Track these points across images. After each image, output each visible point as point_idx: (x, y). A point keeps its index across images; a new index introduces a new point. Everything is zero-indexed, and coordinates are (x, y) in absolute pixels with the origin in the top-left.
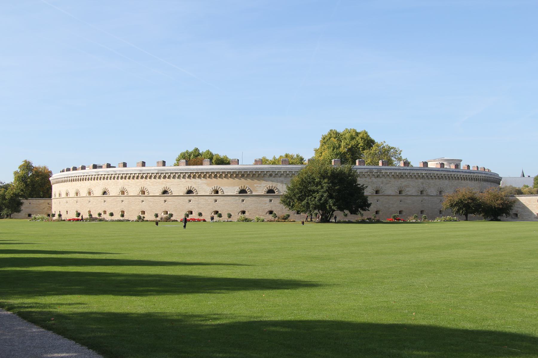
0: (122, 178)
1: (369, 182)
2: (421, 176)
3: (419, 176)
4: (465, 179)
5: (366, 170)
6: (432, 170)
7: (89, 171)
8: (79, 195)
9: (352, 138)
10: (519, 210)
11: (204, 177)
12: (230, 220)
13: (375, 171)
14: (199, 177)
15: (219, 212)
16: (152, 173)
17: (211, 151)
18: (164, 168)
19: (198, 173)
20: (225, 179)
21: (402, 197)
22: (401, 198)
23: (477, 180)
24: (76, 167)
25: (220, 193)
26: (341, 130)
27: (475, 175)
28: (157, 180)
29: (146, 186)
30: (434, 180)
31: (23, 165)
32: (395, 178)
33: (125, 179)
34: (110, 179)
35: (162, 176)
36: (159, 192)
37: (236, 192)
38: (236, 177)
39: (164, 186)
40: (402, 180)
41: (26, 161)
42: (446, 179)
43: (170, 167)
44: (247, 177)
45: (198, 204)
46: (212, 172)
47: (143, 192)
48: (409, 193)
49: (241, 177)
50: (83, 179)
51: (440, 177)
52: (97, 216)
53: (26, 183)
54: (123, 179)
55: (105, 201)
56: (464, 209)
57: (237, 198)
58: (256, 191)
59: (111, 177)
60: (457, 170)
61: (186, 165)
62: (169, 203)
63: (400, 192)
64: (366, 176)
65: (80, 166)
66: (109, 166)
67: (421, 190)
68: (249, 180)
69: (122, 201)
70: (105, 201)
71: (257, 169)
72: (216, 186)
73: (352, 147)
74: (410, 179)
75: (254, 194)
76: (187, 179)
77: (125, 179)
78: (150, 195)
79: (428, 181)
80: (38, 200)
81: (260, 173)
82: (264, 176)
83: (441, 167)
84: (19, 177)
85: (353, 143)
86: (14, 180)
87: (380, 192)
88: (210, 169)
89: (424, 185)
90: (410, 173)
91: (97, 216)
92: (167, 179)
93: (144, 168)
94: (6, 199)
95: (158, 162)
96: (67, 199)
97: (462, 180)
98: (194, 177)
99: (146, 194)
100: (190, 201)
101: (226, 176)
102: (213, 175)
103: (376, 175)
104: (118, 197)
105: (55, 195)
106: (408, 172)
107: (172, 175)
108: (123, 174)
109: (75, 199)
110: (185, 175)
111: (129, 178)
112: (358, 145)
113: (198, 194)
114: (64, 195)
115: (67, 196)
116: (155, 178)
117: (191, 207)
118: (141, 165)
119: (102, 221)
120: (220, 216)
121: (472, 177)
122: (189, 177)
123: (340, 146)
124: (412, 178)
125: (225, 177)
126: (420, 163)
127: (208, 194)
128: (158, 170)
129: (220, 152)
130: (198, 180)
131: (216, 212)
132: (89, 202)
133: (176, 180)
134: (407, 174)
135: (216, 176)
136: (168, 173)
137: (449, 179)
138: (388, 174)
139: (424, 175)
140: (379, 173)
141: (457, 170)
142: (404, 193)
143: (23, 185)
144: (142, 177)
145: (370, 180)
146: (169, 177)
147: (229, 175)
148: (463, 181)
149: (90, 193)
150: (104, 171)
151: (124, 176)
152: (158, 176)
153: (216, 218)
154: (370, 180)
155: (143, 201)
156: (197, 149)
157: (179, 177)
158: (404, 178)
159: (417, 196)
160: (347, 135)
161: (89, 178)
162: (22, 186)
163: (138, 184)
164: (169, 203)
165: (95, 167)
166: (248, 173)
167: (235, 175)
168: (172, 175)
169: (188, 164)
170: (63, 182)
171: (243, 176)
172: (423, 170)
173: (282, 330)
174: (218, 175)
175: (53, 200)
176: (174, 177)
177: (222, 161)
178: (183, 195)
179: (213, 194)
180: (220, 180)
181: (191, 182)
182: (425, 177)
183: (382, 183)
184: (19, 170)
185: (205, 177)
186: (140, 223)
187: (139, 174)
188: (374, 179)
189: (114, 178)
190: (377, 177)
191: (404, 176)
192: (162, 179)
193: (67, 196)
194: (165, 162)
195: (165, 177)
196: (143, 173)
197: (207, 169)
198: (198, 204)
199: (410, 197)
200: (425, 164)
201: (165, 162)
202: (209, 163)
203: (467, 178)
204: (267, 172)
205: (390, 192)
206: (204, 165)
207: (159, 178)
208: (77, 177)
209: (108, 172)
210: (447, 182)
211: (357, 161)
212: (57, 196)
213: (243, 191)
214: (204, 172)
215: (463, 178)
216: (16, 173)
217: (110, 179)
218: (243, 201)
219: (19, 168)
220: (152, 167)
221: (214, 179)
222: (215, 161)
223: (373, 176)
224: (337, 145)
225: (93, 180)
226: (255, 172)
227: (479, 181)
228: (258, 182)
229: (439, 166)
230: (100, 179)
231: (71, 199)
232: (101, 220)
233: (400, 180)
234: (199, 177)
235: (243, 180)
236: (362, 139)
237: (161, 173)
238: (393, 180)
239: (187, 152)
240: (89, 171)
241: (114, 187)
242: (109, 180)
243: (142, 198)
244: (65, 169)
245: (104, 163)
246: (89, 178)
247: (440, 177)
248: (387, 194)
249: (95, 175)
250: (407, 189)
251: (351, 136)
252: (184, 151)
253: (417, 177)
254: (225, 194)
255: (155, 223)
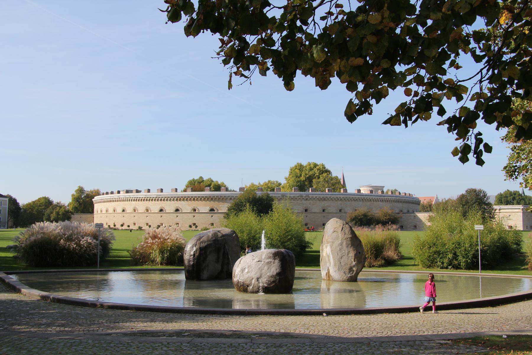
0: (134, 200)
1: (300, 204)
2: (340, 199)
3: (338, 199)
4: (377, 200)
5: (298, 195)
6: (363, 195)
7: (123, 195)
8: (116, 211)
9: (311, 169)
10: (418, 223)
11: (186, 200)
12: (197, 229)
13: (304, 196)
14: (183, 200)
15: (196, 224)
16: (153, 197)
17: (212, 178)
18: (162, 193)
19: (182, 197)
20: (200, 202)
21: (324, 214)
22: (324, 214)
23: (387, 202)
24: (108, 192)
25: (197, 211)
26: (304, 163)
27: (386, 198)
28: (157, 202)
29: (149, 206)
30: (351, 202)
31: (78, 190)
32: (319, 200)
33: (136, 201)
34: (127, 201)
35: (160, 199)
36: (157, 211)
37: (207, 211)
38: (207, 200)
39: (160, 206)
40: (325, 202)
41: (80, 187)
42: (360, 201)
43: (180, 193)
44: (215, 200)
45: (183, 218)
46: (191, 197)
47: (147, 210)
48: (330, 211)
49: (211, 200)
50: (119, 200)
51: (356, 200)
52: (113, 227)
53: (79, 202)
54: (135, 201)
55: (123, 216)
56: (359, 222)
57: (208, 214)
58: (221, 209)
59: (127, 200)
60: (372, 194)
61: (192, 191)
62: (164, 218)
63: (324, 211)
64: (298, 199)
65: (110, 192)
66: (137, 191)
67: (340, 209)
68: (216, 202)
69: (134, 216)
70: (123, 216)
71: (221, 195)
72: (194, 206)
73: (310, 176)
74: (331, 201)
75: (219, 211)
76: (176, 202)
77: (136, 201)
78: (152, 212)
79: (345, 202)
80: (86, 215)
81: (223, 197)
82: (226, 200)
83: (358, 192)
84: (75, 198)
85: (311, 173)
86: (71, 200)
87: (308, 210)
88: (190, 195)
89: (342, 205)
90: (331, 197)
91: (113, 227)
92: (163, 202)
93: (149, 194)
94: (60, 215)
95: (158, 190)
96: (101, 215)
97: (374, 201)
98: (180, 200)
99: (149, 212)
100: (177, 216)
101: (201, 200)
102: (192, 199)
103: (305, 199)
104: (132, 214)
105: (97, 212)
106: (330, 196)
107: (166, 199)
108: (135, 198)
109: (106, 215)
110: (184, 198)
111: (139, 201)
112: (314, 175)
113: (183, 212)
114: (104, 212)
115: (107, 212)
116: (155, 200)
117: (178, 221)
118: (147, 191)
119: (116, 230)
120: (196, 227)
121: (392, 199)
122: (177, 200)
123: (301, 175)
124: (333, 200)
125: (200, 200)
126: (355, 190)
127: (189, 212)
128: (157, 195)
129: (218, 179)
130: (182, 202)
131: (194, 224)
132: (114, 217)
133: (169, 202)
134: (328, 198)
135: (194, 200)
136: (163, 197)
137: (363, 201)
138: (314, 197)
139: (342, 198)
140: (307, 197)
141: (359, 194)
142: (326, 211)
143: (78, 204)
144: (147, 200)
145: (301, 202)
146: (164, 200)
147: (203, 199)
148: (375, 203)
149: (135, 211)
150: (134, 195)
151: (135, 199)
152: (157, 199)
153: (194, 227)
154: (301, 202)
155: (147, 216)
156: (201, 177)
157: (170, 200)
158: (326, 201)
159: (336, 213)
160: (308, 168)
161: (123, 200)
162: (76, 205)
163: (145, 205)
164: (164, 218)
165: (127, 192)
166: (216, 197)
167: (206, 199)
168: (166, 199)
169: (193, 190)
170: (100, 202)
171: (212, 199)
172: (357, 195)
173: (497, 339)
174: (196, 199)
175: (95, 215)
176: (167, 200)
177: (218, 188)
178: (172, 212)
179: (192, 212)
180: (179, 202)
181: (178, 203)
182: (343, 199)
183: (310, 204)
184: (75, 193)
185: (187, 200)
186: (139, 232)
187: (145, 197)
188: (304, 201)
189: (129, 201)
190: (306, 200)
191: (326, 199)
192: (159, 202)
193: (107, 212)
194: (162, 189)
195: (161, 200)
196: (147, 197)
197: (188, 195)
198: (183, 218)
199: (331, 214)
200: (359, 191)
201: (162, 189)
202: (190, 190)
203: (378, 200)
204: (228, 196)
205: (316, 210)
206: (188, 192)
207: (158, 200)
208: (111, 199)
209: (125, 196)
210: (361, 203)
211: (310, 189)
212: (99, 212)
213: (212, 210)
214: (186, 197)
215: (386, 201)
216: (73, 195)
217: (127, 201)
218: (212, 216)
219: (75, 191)
220: (168, 192)
221: (193, 202)
222: (213, 187)
223: (303, 199)
224: (299, 175)
225: (137, 201)
226: (220, 196)
227: (399, 202)
228: (223, 203)
229: (356, 192)
230: (121, 201)
231: (128, 214)
232: (115, 229)
233: (323, 202)
234: (183, 200)
235: (212, 202)
236: (318, 170)
237: (159, 197)
238: (318, 201)
239: (193, 180)
240: (123, 195)
241: (141, 206)
242: (137, 201)
243: (147, 214)
244: (105, 193)
245: (134, 188)
246: (123, 200)
247: (355, 199)
248: (313, 212)
249: (124, 198)
250: (329, 208)
251: (310, 168)
252: (191, 179)
253: (336, 199)
254: (200, 212)
255: (130, 231)
